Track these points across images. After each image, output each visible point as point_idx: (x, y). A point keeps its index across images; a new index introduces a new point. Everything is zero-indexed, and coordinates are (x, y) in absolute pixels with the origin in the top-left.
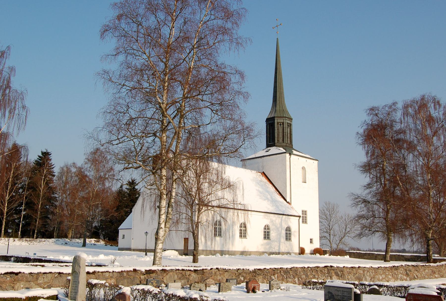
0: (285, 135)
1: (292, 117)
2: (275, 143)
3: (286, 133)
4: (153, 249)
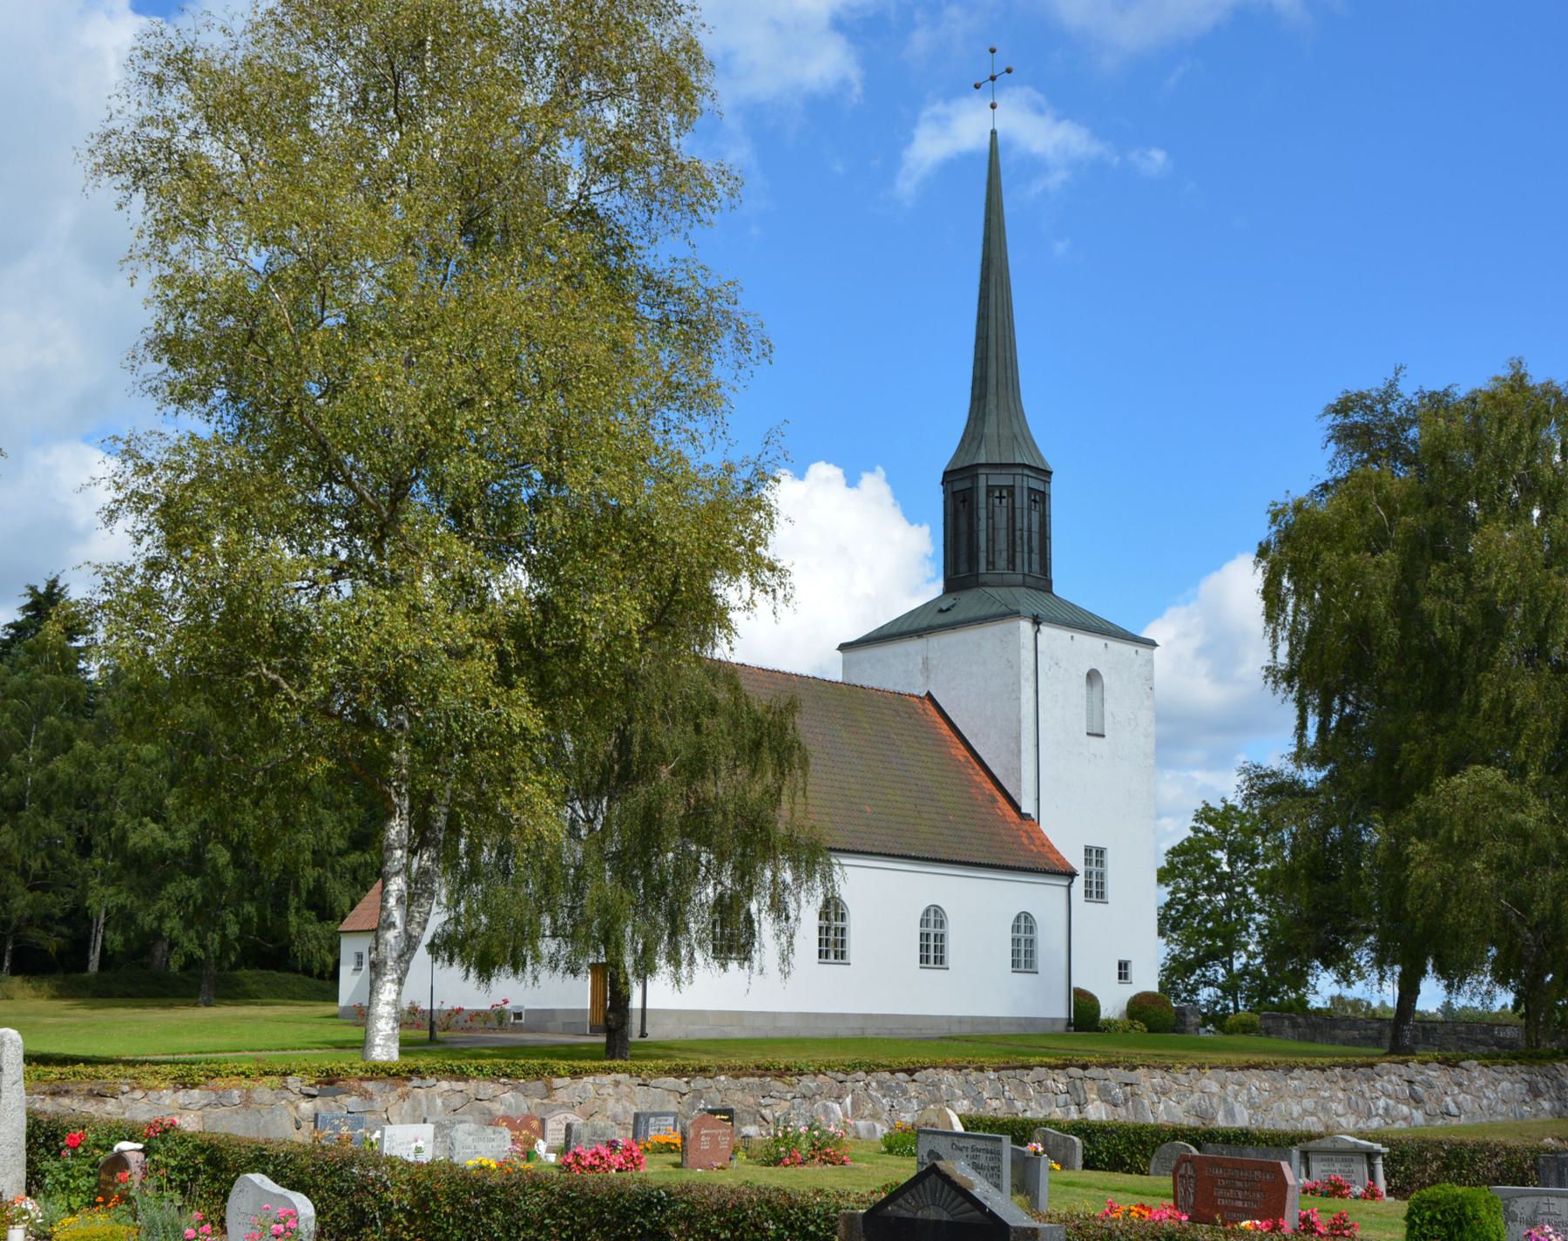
0: (1018, 541)
1: (1051, 462)
2: (978, 575)
3: (1022, 530)
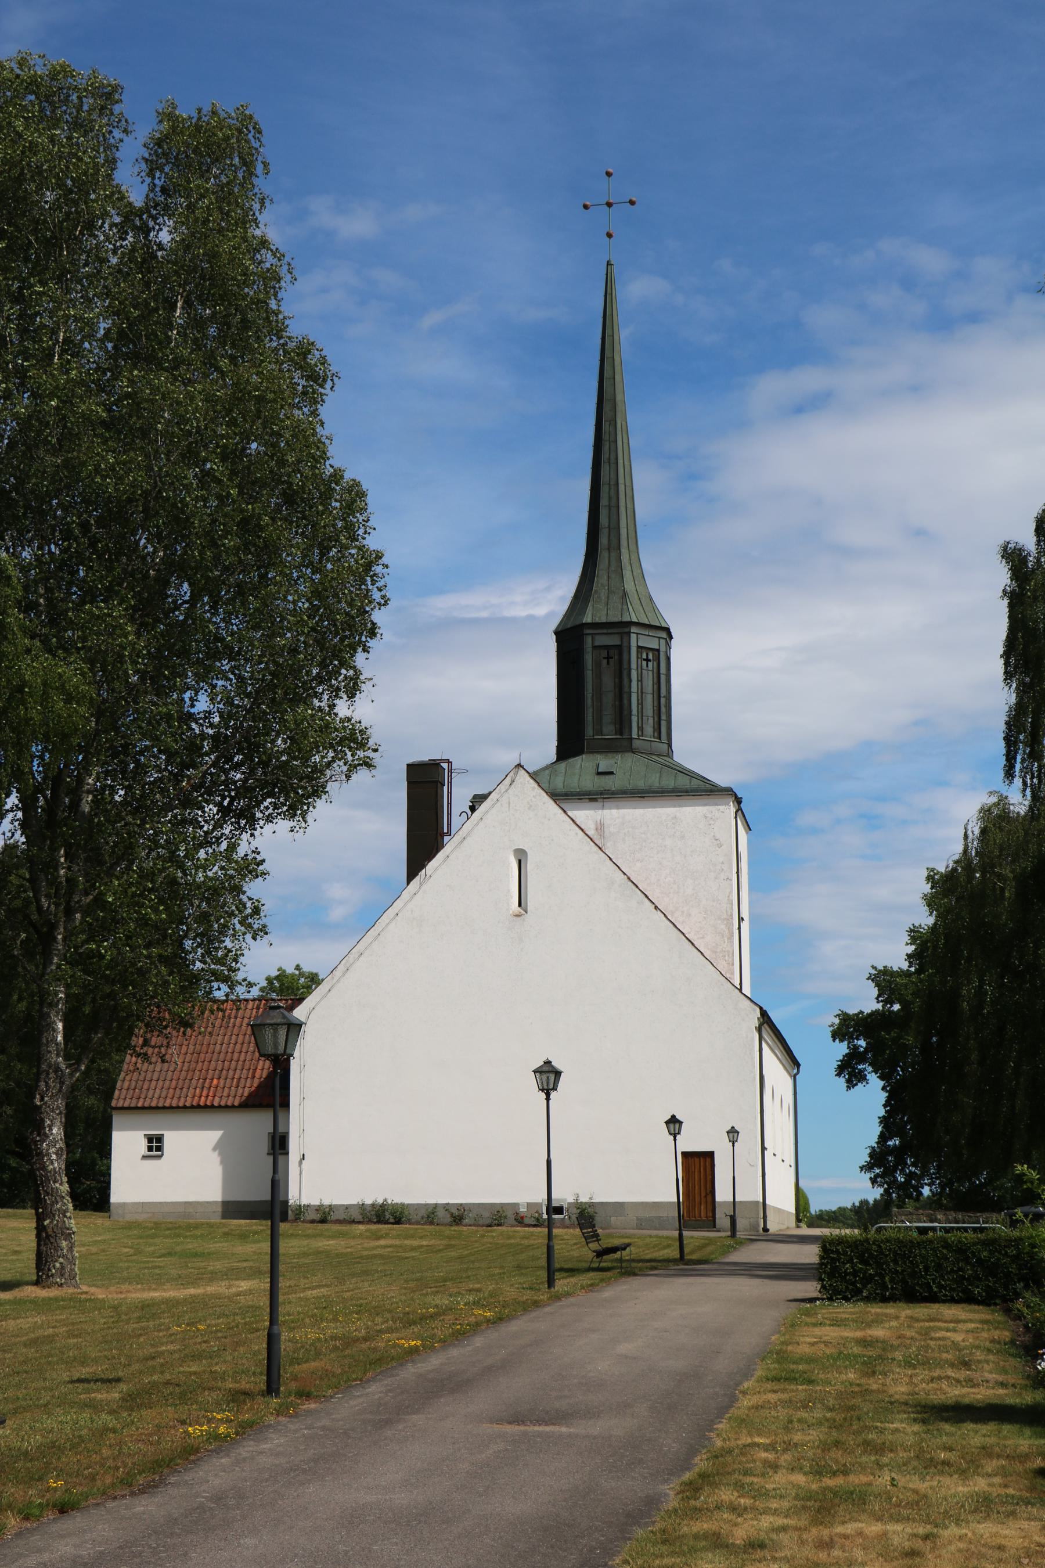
4: (266, 1201)
